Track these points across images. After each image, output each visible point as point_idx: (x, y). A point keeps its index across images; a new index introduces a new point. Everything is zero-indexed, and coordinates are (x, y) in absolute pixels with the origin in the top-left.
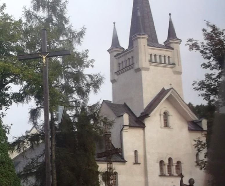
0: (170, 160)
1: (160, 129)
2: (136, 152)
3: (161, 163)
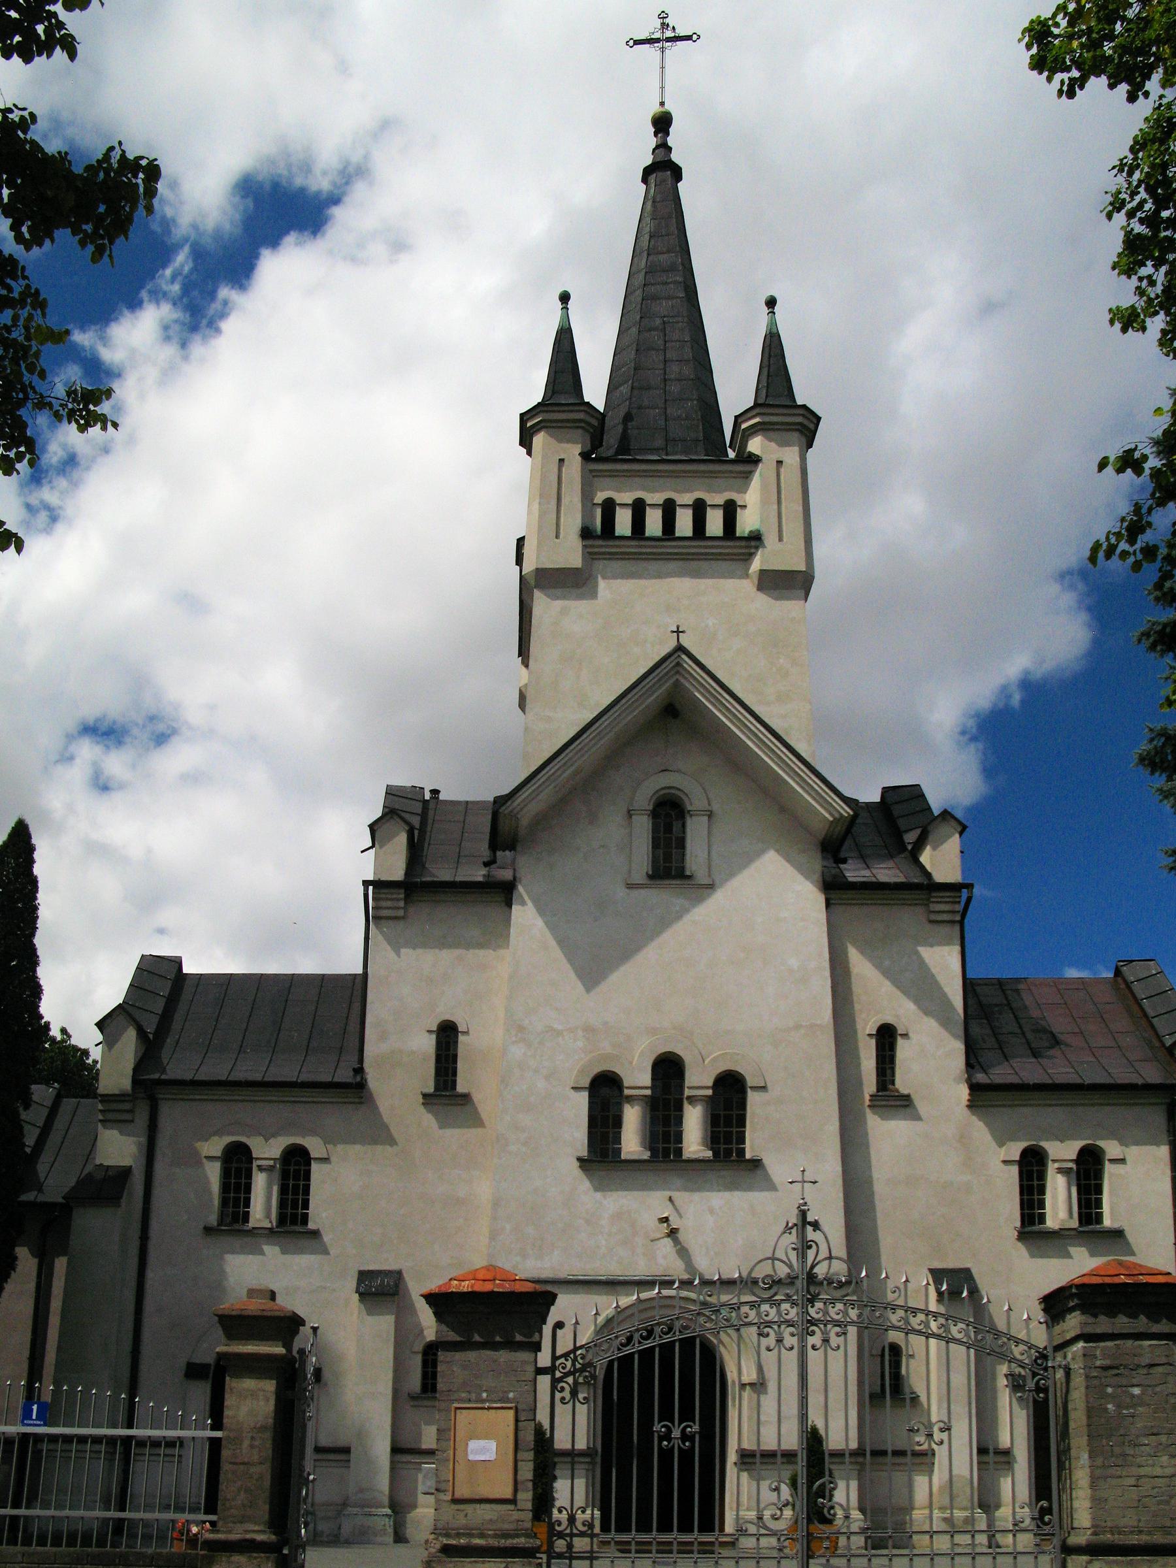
0: (668, 1068)
1: (621, 892)
3: (605, 1090)
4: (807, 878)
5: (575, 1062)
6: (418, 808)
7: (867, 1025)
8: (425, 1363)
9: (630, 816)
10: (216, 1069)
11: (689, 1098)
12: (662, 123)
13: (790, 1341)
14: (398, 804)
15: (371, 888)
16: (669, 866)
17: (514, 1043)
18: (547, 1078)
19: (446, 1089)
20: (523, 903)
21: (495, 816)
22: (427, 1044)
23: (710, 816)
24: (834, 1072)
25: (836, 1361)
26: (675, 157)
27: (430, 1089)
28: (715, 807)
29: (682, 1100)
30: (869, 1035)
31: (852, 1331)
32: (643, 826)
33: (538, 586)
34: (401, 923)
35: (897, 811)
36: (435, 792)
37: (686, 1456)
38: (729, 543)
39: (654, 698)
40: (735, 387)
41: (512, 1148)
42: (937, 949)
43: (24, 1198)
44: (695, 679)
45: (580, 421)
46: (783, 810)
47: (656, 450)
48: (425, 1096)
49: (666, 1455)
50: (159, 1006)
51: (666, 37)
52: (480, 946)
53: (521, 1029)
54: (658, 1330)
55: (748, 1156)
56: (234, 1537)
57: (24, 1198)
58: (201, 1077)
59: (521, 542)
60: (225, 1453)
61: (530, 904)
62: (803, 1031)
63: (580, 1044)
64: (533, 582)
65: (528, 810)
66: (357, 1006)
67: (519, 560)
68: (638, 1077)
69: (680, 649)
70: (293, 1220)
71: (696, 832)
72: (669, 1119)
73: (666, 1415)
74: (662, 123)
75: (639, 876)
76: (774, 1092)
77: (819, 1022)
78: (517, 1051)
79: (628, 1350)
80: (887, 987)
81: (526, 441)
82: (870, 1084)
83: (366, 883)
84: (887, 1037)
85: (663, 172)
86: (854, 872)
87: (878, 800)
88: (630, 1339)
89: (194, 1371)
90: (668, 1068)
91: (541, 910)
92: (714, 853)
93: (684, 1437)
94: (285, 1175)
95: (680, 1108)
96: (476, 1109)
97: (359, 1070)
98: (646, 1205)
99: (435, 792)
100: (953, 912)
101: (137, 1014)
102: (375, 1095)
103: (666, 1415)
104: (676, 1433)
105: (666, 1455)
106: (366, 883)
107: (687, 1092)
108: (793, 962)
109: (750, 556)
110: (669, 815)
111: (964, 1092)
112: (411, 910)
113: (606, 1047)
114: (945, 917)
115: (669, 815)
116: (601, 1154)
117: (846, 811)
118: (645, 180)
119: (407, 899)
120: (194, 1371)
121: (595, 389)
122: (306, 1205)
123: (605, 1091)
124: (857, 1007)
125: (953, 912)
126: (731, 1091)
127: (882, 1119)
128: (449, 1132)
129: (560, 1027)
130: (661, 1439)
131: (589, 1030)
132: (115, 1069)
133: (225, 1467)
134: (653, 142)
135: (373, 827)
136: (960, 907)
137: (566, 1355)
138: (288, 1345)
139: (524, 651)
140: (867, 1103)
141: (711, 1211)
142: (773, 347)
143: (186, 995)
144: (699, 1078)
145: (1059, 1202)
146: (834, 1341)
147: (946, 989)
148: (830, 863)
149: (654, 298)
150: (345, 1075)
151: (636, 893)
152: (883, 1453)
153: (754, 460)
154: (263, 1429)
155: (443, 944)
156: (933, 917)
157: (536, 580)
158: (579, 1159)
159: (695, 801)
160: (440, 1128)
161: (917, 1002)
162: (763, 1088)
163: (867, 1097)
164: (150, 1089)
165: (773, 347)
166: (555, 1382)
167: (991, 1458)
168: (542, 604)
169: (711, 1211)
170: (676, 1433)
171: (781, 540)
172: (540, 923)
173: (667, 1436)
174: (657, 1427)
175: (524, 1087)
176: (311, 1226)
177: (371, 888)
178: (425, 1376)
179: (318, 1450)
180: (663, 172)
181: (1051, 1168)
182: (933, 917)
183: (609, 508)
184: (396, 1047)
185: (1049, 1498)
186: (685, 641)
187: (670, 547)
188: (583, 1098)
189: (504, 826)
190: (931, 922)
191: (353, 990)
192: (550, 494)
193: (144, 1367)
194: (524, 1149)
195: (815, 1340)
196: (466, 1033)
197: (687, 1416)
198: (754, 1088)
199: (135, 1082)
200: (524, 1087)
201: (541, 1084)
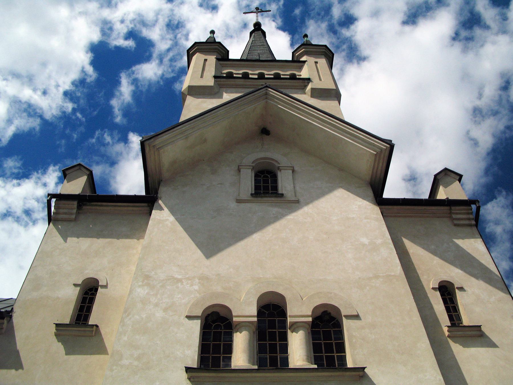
1: (233, 205)
3: (216, 327)
4: (364, 198)
7: (429, 283)
9: (239, 170)
11: (293, 324)
15: (54, 200)
16: (266, 184)
17: (139, 286)
18: (165, 310)
20: (161, 209)
22: (70, 295)
23: (293, 171)
24: (414, 304)
29: (285, 327)
30: (433, 288)
33: (190, 94)
34: (72, 224)
38: (292, 81)
41: (125, 362)
42: (466, 240)
44: (278, 99)
45: (216, 49)
52: (127, 237)
53: (147, 277)
55: (350, 365)
61: (166, 209)
62: (382, 280)
63: (196, 287)
64: (186, 93)
76: (367, 319)
77: (393, 274)
78: (141, 292)
80: (436, 261)
82: (444, 320)
84: (447, 291)
87: (348, 367)
91: (173, 211)
92: (297, 188)
95: (284, 338)
96: (102, 340)
100: (469, 219)
102: (16, 328)
107: (289, 320)
108: (365, 240)
109: (306, 86)
114: (467, 222)
119: (79, 207)
124: (419, 272)
125: (469, 219)
126: (327, 328)
127: (464, 347)
128: (72, 357)
129: (180, 277)
136: (472, 216)
140: (447, 334)
144: (299, 310)
147: (483, 262)
151: (242, 205)
155: (99, 235)
156: (456, 222)
157: (188, 92)
158: (188, 370)
160: (66, 354)
161: (462, 268)
162: (357, 317)
163: (446, 329)
171: (320, 80)
172: (172, 218)
175: (144, 316)
177: (54, 200)
182: (456, 222)
188: (196, 326)
190: (455, 225)
194: (136, 363)
196: (106, 287)
198: (348, 317)
200: (144, 316)
201: (159, 314)
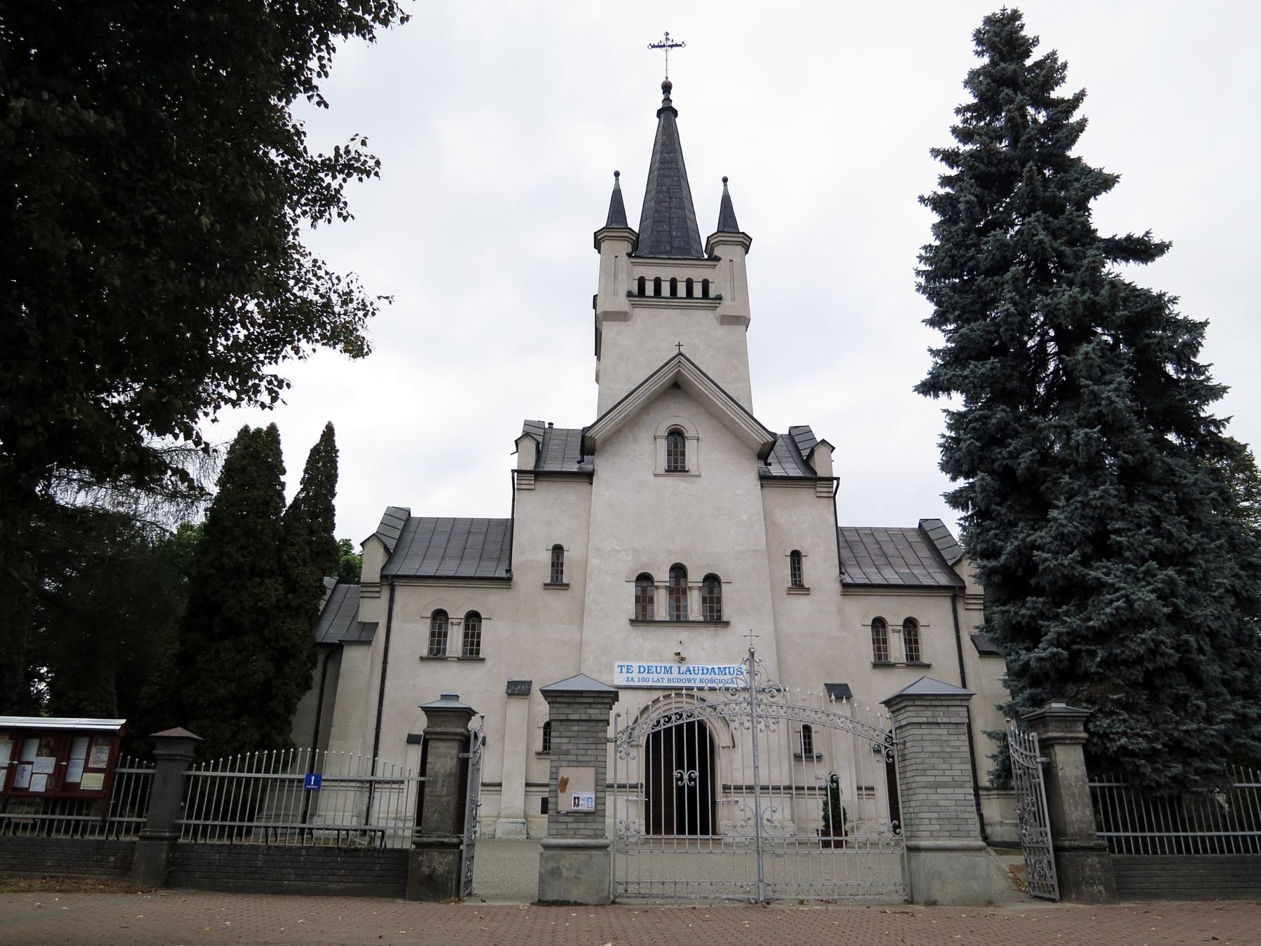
0: (679, 571)
2: (558, 550)
5: (628, 567)
6: (541, 432)
8: (545, 734)
10: (429, 569)
12: (667, 88)
13: (748, 724)
14: (531, 430)
19: (557, 581)
21: (583, 437)
22: (547, 557)
25: (774, 738)
26: (674, 105)
27: (549, 581)
28: (700, 436)
31: (783, 722)
32: (663, 445)
35: (797, 439)
36: (551, 424)
37: (692, 790)
39: (666, 377)
40: (707, 223)
43: (123, 721)
46: (737, 437)
47: (667, 253)
48: (546, 585)
49: (681, 789)
50: (397, 534)
51: (667, 45)
54: (674, 718)
56: (432, 840)
57: (123, 721)
58: (419, 574)
59: (595, 297)
60: (427, 790)
65: (599, 434)
66: (508, 536)
67: (595, 307)
68: (662, 576)
69: (680, 354)
70: (472, 652)
71: (690, 447)
72: (681, 596)
73: (680, 766)
74: (667, 88)
75: (661, 470)
79: (657, 729)
81: (597, 245)
83: (513, 471)
85: (667, 113)
86: (775, 470)
88: (658, 722)
89: (412, 740)
90: (679, 571)
93: (691, 779)
94: (467, 627)
97: (509, 571)
98: (665, 641)
99: (551, 424)
101: (385, 540)
103: (680, 766)
104: (686, 777)
105: (681, 789)
106: (513, 471)
108: (745, 517)
110: (676, 435)
111: (838, 586)
112: (539, 485)
113: (644, 559)
115: (676, 435)
116: (643, 618)
117: (771, 439)
118: (658, 116)
119: (536, 480)
120: (412, 740)
121: (634, 222)
122: (478, 644)
123: (644, 584)
126: (712, 581)
130: (678, 780)
131: (635, 550)
132: (371, 572)
133: (427, 798)
134: (662, 97)
135: (517, 442)
137: (623, 732)
138: (465, 727)
139: (598, 353)
141: (704, 649)
142: (726, 203)
143: (412, 528)
144: (695, 577)
145: (897, 647)
146: (772, 727)
148: (762, 464)
149: (664, 176)
150: (502, 573)
152: (803, 788)
153: (718, 259)
154: (449, 775)
159: (690, 432)
164: (390, 581)
165: (726, 203)
166: (617, 747)
167: (864, 792)
168: (609, 329)
169: (704, 649)
170: (686, 777)
173: (681, 779)
174: (675, 773)
176: (481, 656)
178: (545, 741)
179: (484, 785)
180: (667, 113)
181: (889, 629)
183: (642, 282)
184: (530, 556)
185: (899, 820)
186: (683, 350)
187: (674, 302)
189: (587, 443)
191: (507, 527)
192: (607, 273)
193: (382, 736)
195: (762, 726)
197: (691, 766)
199: (382, 577)
